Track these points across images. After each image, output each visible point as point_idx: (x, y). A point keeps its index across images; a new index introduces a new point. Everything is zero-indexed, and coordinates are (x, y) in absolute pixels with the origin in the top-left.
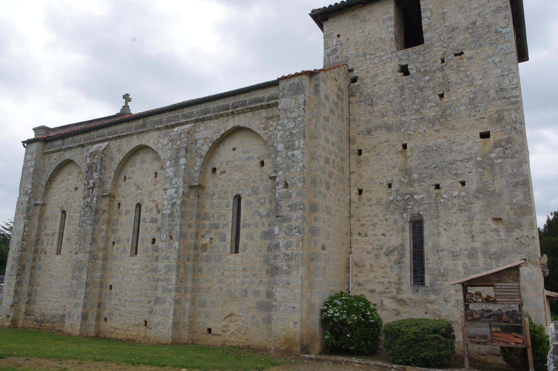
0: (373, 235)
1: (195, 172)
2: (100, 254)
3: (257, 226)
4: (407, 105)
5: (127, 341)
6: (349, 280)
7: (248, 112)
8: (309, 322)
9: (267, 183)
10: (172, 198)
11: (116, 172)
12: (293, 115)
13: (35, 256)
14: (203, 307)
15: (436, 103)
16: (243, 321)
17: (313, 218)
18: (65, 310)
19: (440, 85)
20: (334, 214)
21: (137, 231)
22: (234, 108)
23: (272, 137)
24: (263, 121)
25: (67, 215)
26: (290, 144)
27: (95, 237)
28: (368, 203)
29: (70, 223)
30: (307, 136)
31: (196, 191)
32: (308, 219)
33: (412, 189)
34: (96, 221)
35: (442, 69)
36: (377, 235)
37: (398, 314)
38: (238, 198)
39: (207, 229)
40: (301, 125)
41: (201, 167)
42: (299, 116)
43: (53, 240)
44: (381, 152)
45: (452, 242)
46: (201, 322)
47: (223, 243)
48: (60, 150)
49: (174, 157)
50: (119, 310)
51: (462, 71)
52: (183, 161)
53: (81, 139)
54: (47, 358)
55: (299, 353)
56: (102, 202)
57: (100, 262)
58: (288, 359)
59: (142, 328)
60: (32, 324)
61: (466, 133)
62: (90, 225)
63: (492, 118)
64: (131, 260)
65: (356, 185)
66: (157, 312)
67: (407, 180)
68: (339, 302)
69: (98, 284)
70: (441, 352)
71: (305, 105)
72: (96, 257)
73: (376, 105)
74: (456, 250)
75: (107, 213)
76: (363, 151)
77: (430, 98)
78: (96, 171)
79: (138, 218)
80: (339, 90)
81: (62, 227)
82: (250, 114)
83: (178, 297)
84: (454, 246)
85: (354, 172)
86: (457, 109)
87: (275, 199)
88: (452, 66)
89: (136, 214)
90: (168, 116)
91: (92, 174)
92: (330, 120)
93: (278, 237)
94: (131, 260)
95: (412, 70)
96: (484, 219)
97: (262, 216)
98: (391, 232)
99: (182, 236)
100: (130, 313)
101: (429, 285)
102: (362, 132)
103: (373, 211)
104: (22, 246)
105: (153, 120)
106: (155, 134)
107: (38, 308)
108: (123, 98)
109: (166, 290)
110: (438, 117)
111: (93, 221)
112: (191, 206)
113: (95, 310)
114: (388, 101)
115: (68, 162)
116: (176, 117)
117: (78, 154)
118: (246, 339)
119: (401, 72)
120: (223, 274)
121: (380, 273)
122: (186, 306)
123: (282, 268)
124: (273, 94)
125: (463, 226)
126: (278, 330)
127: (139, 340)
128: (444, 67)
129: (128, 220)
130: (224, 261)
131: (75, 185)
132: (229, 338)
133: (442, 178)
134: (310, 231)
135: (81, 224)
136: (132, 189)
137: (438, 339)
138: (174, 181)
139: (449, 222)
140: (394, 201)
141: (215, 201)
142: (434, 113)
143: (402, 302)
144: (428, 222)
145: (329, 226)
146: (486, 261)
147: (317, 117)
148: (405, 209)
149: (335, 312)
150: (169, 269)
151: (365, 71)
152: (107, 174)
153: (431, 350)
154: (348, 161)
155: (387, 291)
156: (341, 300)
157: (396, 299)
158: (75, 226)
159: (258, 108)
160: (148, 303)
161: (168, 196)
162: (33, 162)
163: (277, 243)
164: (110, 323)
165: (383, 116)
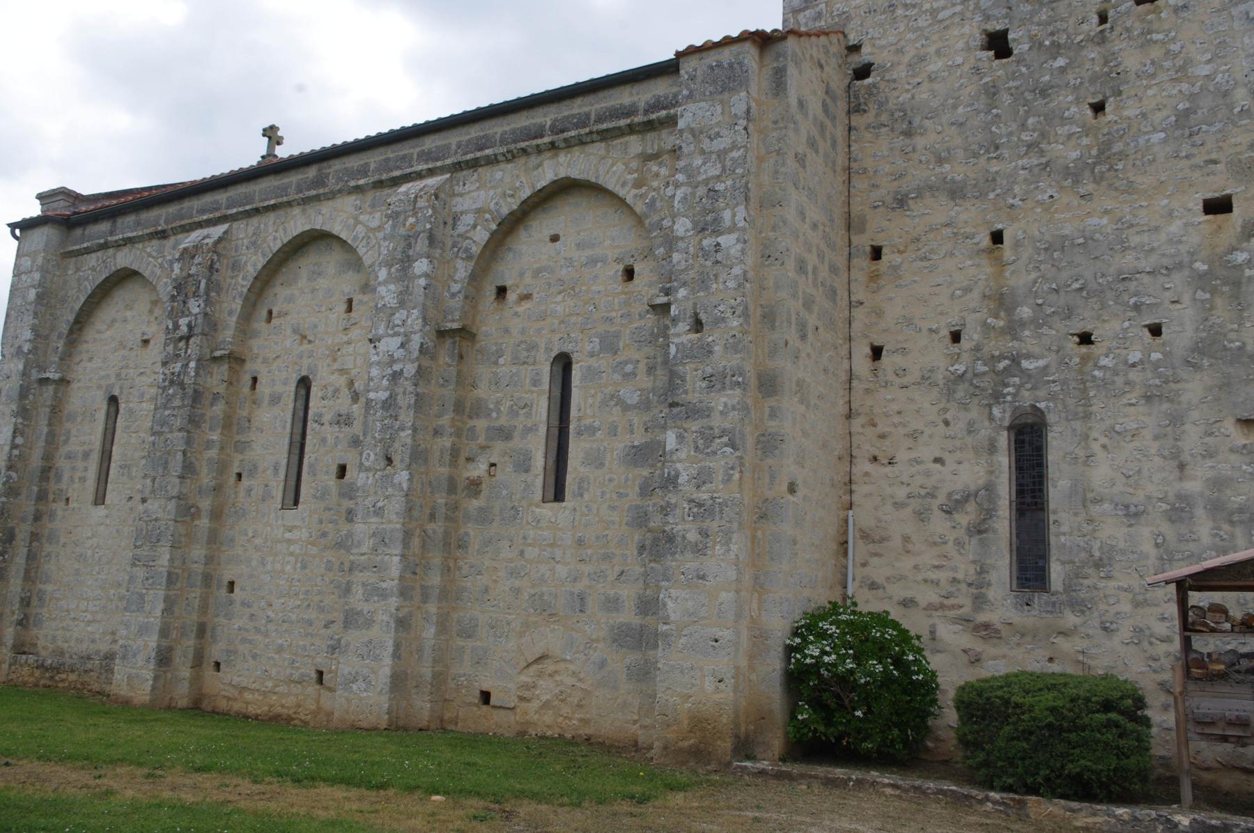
0: (910, 460)
1: (453, 295)
2: (205, 504)
3: (613, 431)
4: (1004, 131)
5: (271, 719)
6: (845, 575)
7: (593, 142)
8: (754, 677)
9: (642, 323)
10: (392, 360)
11: (246, 299)
12: (719, 144)
13: (40, 507)
14: (470, 637)
15: (1083, 126)
16: (574, 673)
17: (767, 411)
18: (115, 641)
19: (1094, 79)
20: (815, 404)
21: (299, 447)
22: (557, 134)
23: (658, 204)
24: (634, 165)
25: (122, 406)
26: (709, 218)
27: (193, 460)
28: (898, 381)
29: (128, 427)
30: (752, 200)
31: (454, 343)
32: (753, 412)
33: (1016, 344)
34: (194, 421)
35: (1101, 39)
36: (922, 462)
37: (976, 660)
38: (564, 363)
39: (481, 440)
40: (737, 171)
41: (468, 284)
42: (734, 147)
43: (86, 469)
44: (932, 251)
45: (1124, 480)
46: (464, 675)
47: (524, 476)
48: (104, 246)
49: (400, 257)
50: (250, 642)
51: (1156, 42)
52: (421, 266)
53: (159, 217)
54: (63, 759)
55: (728, 758)
56: (211, 374)
57: (204, 523)
58: (701, 771)
59: (310, 689)
60: (32, 675)
61: (1166, 202)
62: (180, 430)
63: (1240, 161)
64: (283, 518)
65: (866, 336)
66: (352, 647)
67: (1002, 323)
68: (834, 627)
69: (200, 578)
70: (1125, 762)
71: (748, 120)
72: (193, 510)
73: (922, 134)
74: (1134, 500)
75: (224, 402)
76: (884, 251)
77: (1067, 114)
78: (196, 295)
79: (301, 414)
80: (827, 93)
81: (109, 437)
82: (598, 148)
83: (406, 610)
84: (1131, 491)
85: (862, 303)
86: (1142, 141)
87: (666, 362)
88: (1128, 30)
89: (298, 404)
90: (383, 157)
91: (184, 302)
92: (807, 164)
93: (675, 458)
94: (283, 518)
95: (1019, 44)
96: (1213, 420)
97: (626, 408)
98: (958, 455)
99: (418, 456)
100: (280, 650)
101: (1061, 589)
102: (883, 202)
103: (912, 400)
104: (7, 481)
105: (343, 166)
106: (348, 203)
107: (46, 636)
108: (264, 135)
109: (374, 592)
110: (1090, 161)
111: (185, 421)
112: (441, 381)
113: (190, 642)
114: (953, 124)
115: (126, 276)
116: (404, 157)
117: (150, 255)
118: (581, 720)
119: (989, 48)
120: (522, 553)
121: (929, 557)
122: (424, 635)
123: (684, 537)
124: (660, 97)
125: (1156, 438)
126: (672, 697)
127: (303, 718)
128: (1107, 34)
129: (276, 418)
130: (524, 522)
131: (143, 334)
132: (536, 717)
133: (1099, 318)
134: (758, 442)
135: (157, 428)
136: (288, 343)
137: (1117, 726)
138: (399, 317)
139: (1118, 428)
140: (969, 375)
141: (502, 371)
142: (1078, 152)
143: (986, 631)
144: (1060, 429)
145: (805, 434)
146: (1219, 528)
147: (778, 152)
148: (997, 397)
149: (824, 653)
150: (382, 540)
151: (892, 48)
152: (225, 305)
153: (1098, 754)
154: (846, 275)
155: (946, 602)
156: (837, 623)
157: (971, 625)
158: (142, 435)
159: (620, 133)
160: (326, 626)
161: (381, 354)
162: (37, 276)
163: (673, 473)
164: (227, 674)
165: (940, 161)
